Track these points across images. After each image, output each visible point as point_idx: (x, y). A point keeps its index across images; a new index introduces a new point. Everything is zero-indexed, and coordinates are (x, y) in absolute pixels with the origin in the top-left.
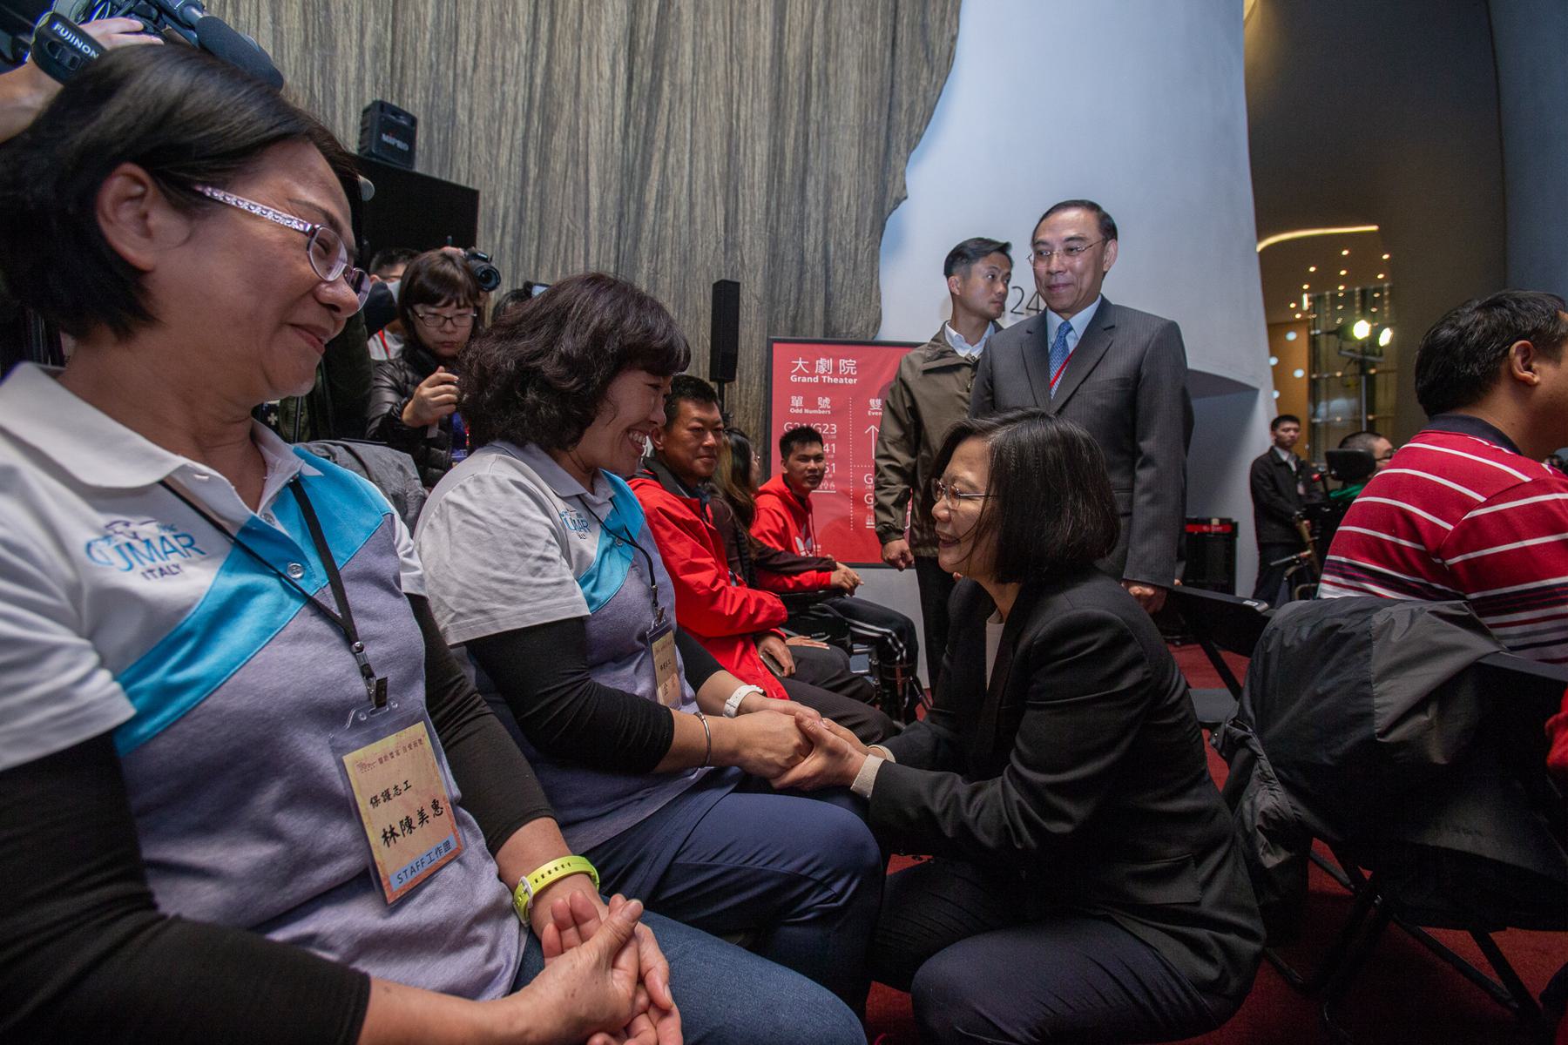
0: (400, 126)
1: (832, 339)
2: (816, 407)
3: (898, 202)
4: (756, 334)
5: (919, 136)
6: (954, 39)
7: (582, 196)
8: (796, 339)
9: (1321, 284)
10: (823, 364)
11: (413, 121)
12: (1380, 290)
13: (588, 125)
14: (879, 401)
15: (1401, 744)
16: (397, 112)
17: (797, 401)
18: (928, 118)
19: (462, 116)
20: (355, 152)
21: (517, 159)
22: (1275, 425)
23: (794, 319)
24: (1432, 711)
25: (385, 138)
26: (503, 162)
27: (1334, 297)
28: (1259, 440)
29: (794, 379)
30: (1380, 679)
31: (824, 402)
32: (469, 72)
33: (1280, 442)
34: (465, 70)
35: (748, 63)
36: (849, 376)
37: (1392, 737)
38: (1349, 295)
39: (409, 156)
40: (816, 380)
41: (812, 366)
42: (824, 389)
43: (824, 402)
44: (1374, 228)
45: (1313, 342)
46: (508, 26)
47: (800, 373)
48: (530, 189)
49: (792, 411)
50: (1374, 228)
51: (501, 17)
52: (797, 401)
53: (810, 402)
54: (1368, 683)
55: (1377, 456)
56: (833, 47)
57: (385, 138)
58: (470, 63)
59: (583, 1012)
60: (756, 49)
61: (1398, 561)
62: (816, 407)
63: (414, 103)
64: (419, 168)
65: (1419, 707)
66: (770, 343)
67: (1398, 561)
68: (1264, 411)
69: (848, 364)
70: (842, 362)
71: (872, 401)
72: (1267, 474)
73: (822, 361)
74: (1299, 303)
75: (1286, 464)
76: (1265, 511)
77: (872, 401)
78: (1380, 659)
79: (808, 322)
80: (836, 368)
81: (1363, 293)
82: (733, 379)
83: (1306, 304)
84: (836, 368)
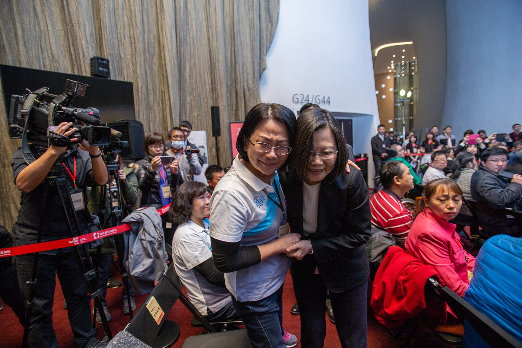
0: (104, 64)
3: (264, 70)
5: (270, 47)
6: (278, 14)
7: (165, 80)
9: (398, 60)
11: (108, 61)
12: (414, 62)
13: (165, 56)
15: (376, 262)
16: (103, 59)
18: (271, 42)
19: (123, 55)
20: (89, 75)
21: (143, 69)
22: (379, 127)
24: (381, 255)
25: (100, 69)
26: (138, 70)
27: (401, 65)
28: (374, 131)
30: (373, 249)
32: (123, 40)
33: (379, 133)
34: (121, 39)
35: (214, 28)
37: (374, 261)
38: (405, 64)
39: (108, 73)
44: (411, 43)
45: (395, 79)
46: (134, 22)
48: (148, 78)
50: (411, 43)
51: (131, 19)
54: (371, 250)
55: (398, 151)
56: (241, 19)
57: (100, 69)
58: (123, 37)
60: (216, 23)
63: (106, 55)
64: (112, 78)
65: (379, 255)
66: (230, 123)
68: (376, 122)
72: (375, 141)
74: (391, 67)
75: (380, 139)
76: (375, 153)
78: (373, 245)
81: (410, 63)
83: (393, 67)
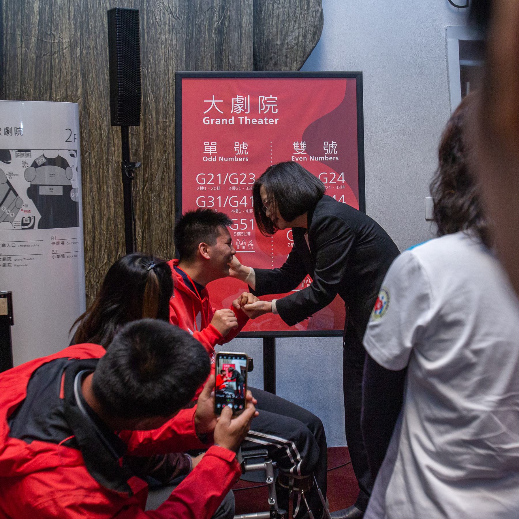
1: (264, 64)
2: (322, 153)
4: (172, 55)
8: (224, 73)
10: (240, 103)
14: (303, 145)
17: (210, 148)
23: (220, 30)
29: (206, 121)
31: (242, 147)
36: (270, 115)
40: (232, 121)
41: (226, 105)
42: (242, 131)
43: (242, 147)
47: (213, 114)
49: (205, 159)
52: (210, 148)
53: (225, 149)
59: (478, 247)
61: (90, 305)
62: (322, 153)
67: (90, 305)
69: (268, 102)
70: (261, 99)
71: (296, 145)
73: (238, 98)
77: (296, 145)
79: (235, 35)
80: (254, 106)
82: (137, 122)
84: (254, 106)
